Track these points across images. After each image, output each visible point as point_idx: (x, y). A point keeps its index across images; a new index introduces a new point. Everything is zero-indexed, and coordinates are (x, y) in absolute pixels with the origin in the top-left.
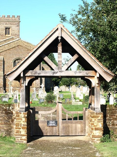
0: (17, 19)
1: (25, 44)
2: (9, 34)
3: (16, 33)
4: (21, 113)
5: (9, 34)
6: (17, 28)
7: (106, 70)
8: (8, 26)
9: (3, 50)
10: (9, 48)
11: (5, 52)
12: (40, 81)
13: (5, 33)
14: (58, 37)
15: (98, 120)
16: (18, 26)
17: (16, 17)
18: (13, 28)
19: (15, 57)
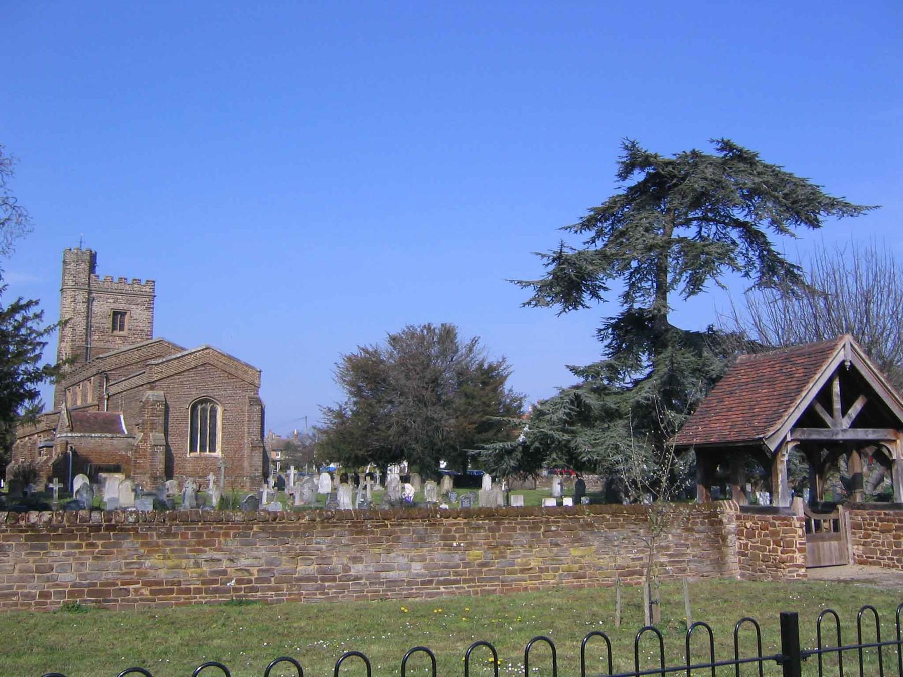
0: (148, 290)
1: (223, 360)
3: (142, 328)
5: (122, 329)
6: (147, 313)
7: (182, 436)
8: (121, 306)
9: (164, 375)
10: (180, 370)
11: (169, 379)
13: (111, 326)
14: (844, 361)
16: (150, 309)
17: (143, 283)
18: (137, 314)
19: (195, 394)
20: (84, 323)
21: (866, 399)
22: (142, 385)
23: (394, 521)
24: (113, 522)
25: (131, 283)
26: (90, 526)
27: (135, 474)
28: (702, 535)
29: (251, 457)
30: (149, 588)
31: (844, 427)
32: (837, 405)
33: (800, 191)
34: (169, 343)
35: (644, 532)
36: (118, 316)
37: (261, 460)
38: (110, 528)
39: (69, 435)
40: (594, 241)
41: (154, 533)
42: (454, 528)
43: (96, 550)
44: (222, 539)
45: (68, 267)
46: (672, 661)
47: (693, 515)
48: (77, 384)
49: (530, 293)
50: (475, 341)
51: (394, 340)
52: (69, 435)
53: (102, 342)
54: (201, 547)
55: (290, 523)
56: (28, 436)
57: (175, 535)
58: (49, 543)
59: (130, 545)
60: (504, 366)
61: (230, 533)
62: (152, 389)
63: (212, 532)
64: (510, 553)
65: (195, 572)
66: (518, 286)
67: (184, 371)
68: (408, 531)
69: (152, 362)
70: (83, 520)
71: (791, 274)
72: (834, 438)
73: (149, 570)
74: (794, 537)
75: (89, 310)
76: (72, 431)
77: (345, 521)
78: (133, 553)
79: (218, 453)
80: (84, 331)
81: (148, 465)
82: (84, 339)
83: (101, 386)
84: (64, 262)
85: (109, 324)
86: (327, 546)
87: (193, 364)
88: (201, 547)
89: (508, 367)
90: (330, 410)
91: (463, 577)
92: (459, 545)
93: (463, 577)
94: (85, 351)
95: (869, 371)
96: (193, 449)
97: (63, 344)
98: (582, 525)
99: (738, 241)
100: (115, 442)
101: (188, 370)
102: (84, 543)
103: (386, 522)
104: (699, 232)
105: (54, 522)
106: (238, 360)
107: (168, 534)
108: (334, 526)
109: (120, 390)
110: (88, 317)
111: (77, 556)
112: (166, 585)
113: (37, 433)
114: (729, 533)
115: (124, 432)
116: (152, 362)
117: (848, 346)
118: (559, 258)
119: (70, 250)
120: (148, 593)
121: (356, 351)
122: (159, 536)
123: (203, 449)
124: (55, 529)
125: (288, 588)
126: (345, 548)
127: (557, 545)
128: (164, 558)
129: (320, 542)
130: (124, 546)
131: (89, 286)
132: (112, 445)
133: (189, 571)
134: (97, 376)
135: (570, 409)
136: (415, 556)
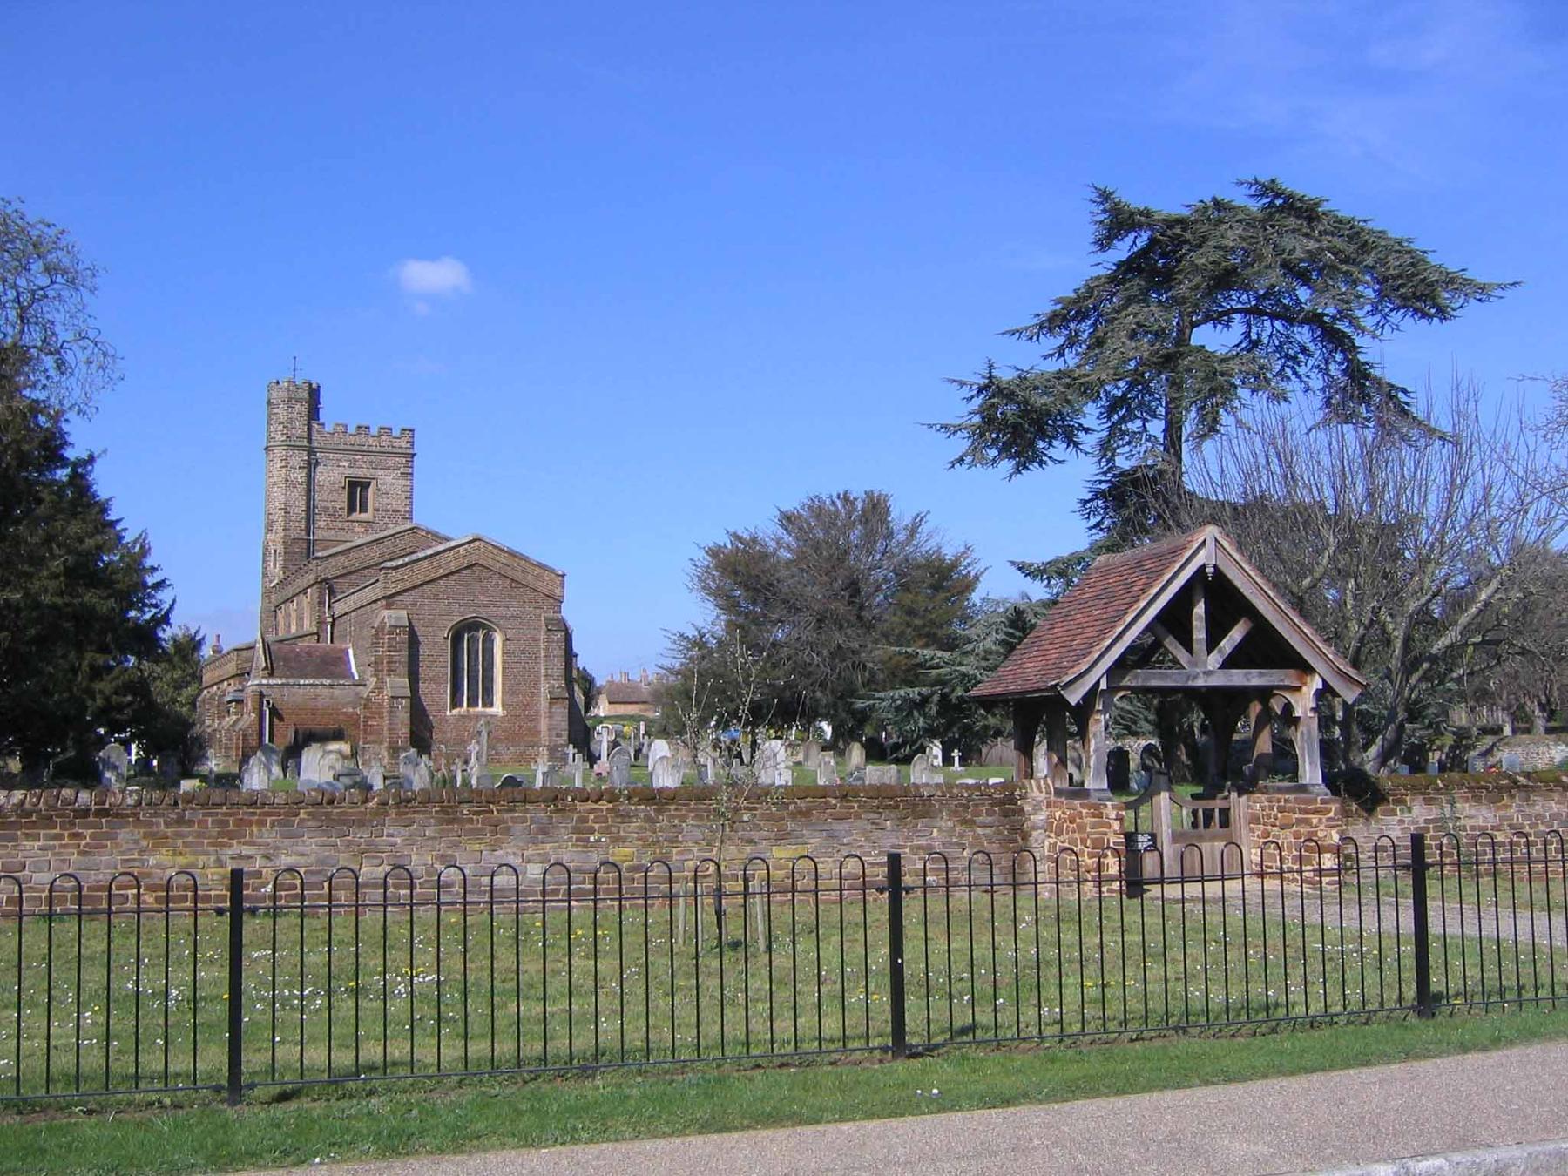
0: (403, 444)
2: (364, 509)
4: (1106, 806)
5: (364, 509)
8: (362, 472)
9: (407, 585)
10: (433, 576)
12: (569, 717)
14: (1203, 567)
15: (1329, 820)
16: (408, 475)
17: (396, 433)
18: (387, 483)
20: (302, 501)
21: (1250, 625)
22: (375, 602)
23: (504, 805)
24: (107, 806)
25: (376, 434)
26: (74, 811)
27: (364, 743)
28: (988, 831)
29: (551, 715)
30: (154, 894)
31: (1210, 668)
32: (1199, 634)
33: (1393, 261)
34: (428, 533)
35: (892, 826)
36: (356, 490)
37: (567, 718)
38: (102, 813)
39: (264, 681)
40: (1062, 355)
41: (161, 820)
42: (592, 816)
43: (83, 843)
44: (255, 829)
45: (275, 411)
46: (190, 915)
47: (974, 800)
48: (290, 600)
49: (961, 444)
50: (918, 521)
51: (788, 520)
52: (264, 681)
53: (333, 532)
54: (226, 840)
55: (351, 808)
56: (216, 684)
57: (190, 823)
58: (19, 833)
59: (129, 836)
60: (969, 560)
61: (228, 821)
62: (388, 607)
63: (241, 819)
64: (678, 853)
65: (218, 874)
66: (943, 435)
67: (441, 578)
68: (524, 820)
69: (388, 564)
70: (66, 802)
71: (1394, 401)
72: (1190, 683)
73: (154, 870)
74: (1106, 834)
75: (310, 479)
76: (271, 675)
77: (430, 805)
78: (132, 846)
79: (497, 709)
80: (304, 514)
81: (385, 728)
82: (303, 527)
83: (322, 602)
84: (269, 403)
85: (342, 500)
86: (403, 841)
87: (453, 567)
88: (226, 840)
89: (975, 561)
90: (683, 637)
91: (605, 886)
92: (599, 840)
93: (605, 886)
94: (305, 545)
95: (1246, 580)
96: (456, 703)
97: (271, 536)
98: (792, 814)
99: (1311, 347)
100: (336, 692)
101: (446, 576)
102: (66, 833)
103: (491, 806)
104: (1247, 335)
105: (27, 806)
106: (526, 559)
107: (180, 821)
108: (414, 812)
109: (347, 610)
110: (309, 490)
111: (57, 850)
112: (178, 891)
113: (227, 679)
114: (1034, 828)
115: (353, 678)
116: (388, 564)
117: (1210, 544)
118: (990, 387)
119: (278, 383)
120: (151, 900)
121: (724, 540)
122: (167, 825)
123: (473, 702)
124: (29, 815)
125: (346, 896)
126: (430, 842)
127: (751, 841)
128: (175, 854)
129: (394, 835)
130: (120, 837)
131: (309, 440)
132: (331, 698)
133: (209, 871)
134: (315, 587)
135: (1007, 634)
136: (533, 855)
